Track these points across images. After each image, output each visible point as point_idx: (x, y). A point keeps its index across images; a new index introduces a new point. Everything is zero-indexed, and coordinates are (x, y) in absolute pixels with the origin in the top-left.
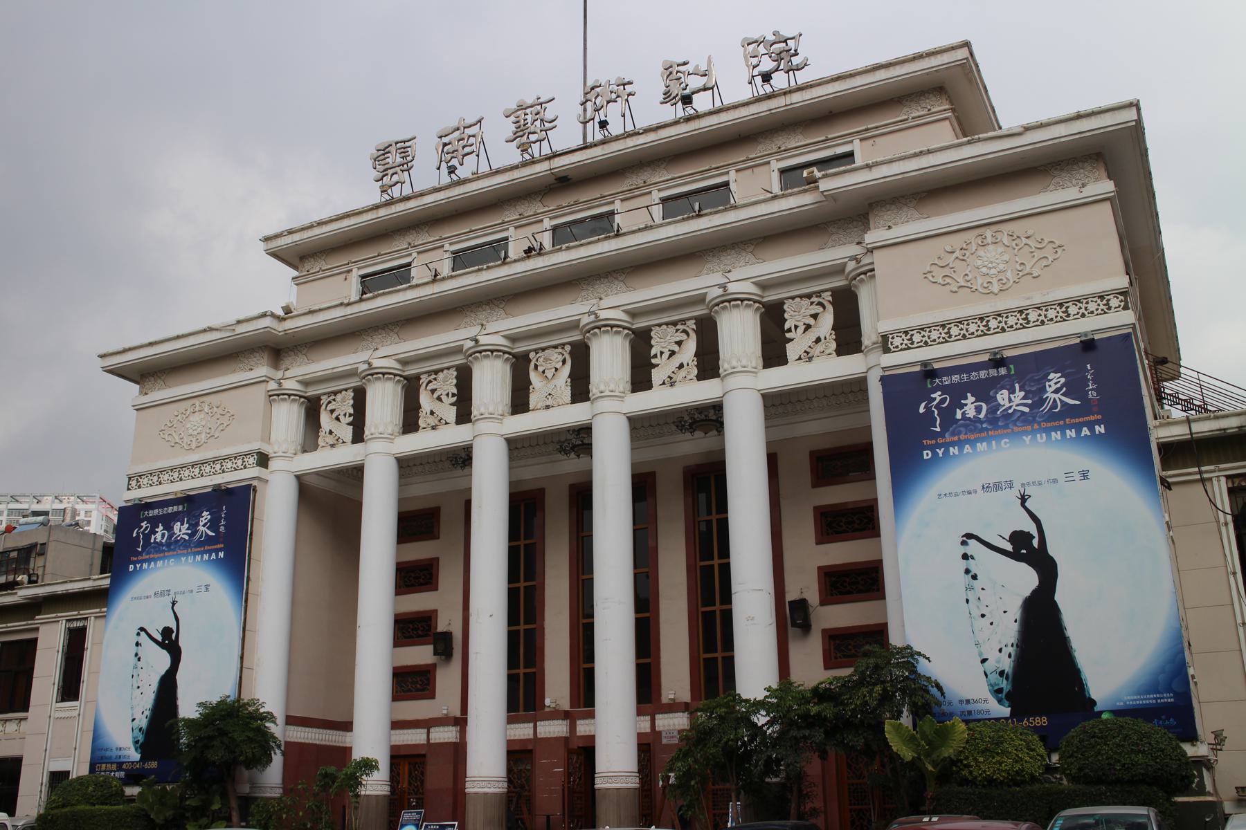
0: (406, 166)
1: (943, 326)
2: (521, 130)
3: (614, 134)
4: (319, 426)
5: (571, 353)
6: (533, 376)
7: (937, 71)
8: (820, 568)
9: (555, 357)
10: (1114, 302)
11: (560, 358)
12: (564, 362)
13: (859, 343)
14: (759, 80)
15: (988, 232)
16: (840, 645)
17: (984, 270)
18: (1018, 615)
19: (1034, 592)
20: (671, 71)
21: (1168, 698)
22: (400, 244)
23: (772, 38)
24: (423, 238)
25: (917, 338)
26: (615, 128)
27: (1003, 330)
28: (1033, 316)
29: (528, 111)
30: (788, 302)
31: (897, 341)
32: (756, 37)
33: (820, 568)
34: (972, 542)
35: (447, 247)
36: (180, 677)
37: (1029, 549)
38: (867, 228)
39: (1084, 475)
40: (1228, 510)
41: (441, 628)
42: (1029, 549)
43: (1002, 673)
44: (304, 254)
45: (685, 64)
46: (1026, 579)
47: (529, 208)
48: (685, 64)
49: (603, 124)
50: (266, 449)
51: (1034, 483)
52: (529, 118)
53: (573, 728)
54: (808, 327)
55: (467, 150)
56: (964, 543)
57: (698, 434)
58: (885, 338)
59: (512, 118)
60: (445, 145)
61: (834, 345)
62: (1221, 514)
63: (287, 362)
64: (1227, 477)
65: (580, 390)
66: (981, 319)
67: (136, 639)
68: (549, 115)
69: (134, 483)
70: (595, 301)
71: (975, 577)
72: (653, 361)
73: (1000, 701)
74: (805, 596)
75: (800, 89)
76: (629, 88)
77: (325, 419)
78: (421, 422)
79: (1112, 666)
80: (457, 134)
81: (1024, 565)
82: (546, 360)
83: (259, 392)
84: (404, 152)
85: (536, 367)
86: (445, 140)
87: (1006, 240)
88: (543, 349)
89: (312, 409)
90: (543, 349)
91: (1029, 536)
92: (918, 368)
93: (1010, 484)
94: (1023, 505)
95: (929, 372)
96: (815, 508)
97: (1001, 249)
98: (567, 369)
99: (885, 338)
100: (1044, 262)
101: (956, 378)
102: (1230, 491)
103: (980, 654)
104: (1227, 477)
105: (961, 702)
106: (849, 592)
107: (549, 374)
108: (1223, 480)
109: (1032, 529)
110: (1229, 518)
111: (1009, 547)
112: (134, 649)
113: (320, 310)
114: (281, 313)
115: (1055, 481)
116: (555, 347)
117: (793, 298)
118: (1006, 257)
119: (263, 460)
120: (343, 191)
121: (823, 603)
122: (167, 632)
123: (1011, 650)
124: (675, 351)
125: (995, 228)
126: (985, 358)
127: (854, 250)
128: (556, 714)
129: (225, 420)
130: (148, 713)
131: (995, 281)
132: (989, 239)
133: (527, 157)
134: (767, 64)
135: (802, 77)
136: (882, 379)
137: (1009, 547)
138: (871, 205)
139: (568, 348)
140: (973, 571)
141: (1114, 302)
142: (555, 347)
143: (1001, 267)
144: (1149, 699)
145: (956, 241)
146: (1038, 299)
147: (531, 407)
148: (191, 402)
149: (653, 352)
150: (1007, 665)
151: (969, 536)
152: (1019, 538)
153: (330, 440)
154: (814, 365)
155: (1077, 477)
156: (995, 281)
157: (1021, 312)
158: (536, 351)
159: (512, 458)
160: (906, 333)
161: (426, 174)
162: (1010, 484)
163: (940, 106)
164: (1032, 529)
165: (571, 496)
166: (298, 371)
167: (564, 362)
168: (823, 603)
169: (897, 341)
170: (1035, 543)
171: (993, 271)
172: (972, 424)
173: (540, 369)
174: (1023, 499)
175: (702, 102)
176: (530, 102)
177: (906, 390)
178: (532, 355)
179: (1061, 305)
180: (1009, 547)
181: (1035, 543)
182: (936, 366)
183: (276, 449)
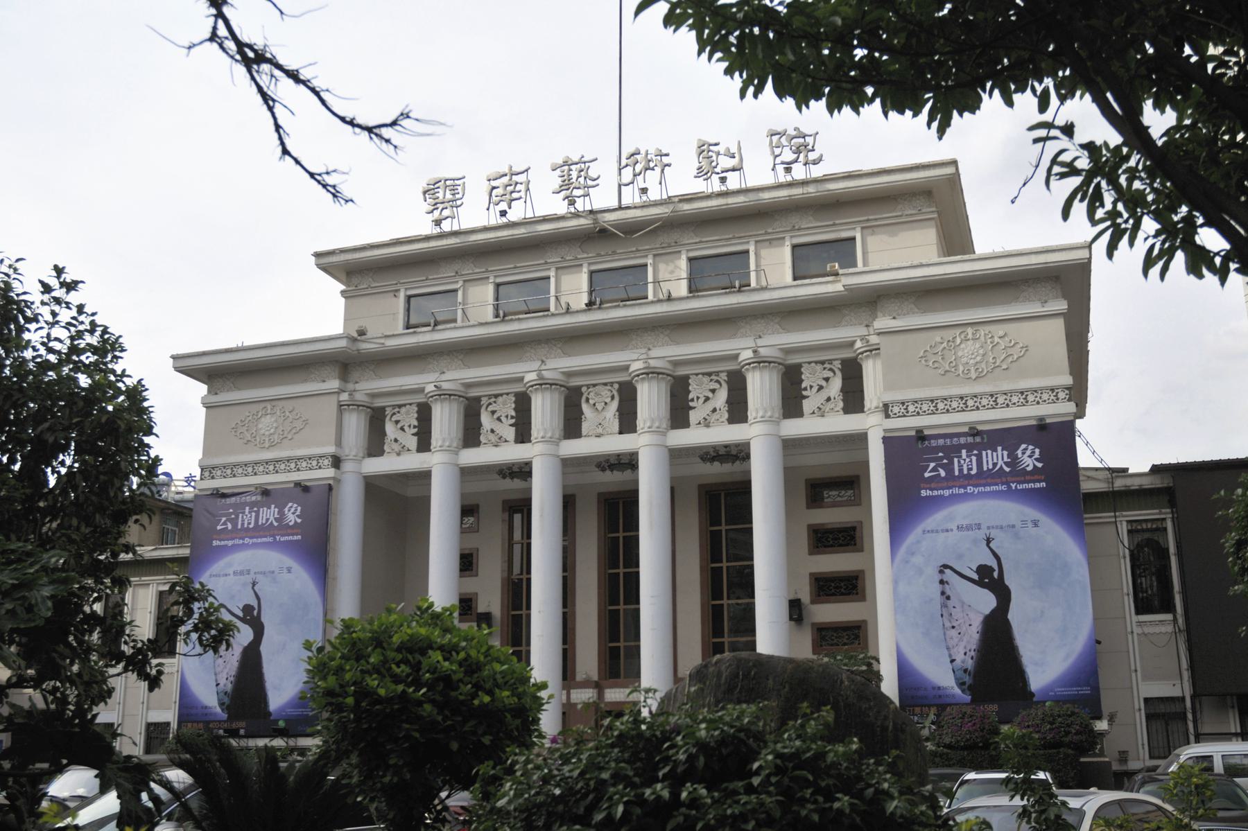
0: (454, 204)
1: (932, 401)
2: (566, 185)
3: (652, 199)
4: (384, 434)
5: (619, 391)
6: (584, 407)
7: (929, 181)
8: (811, 574)
9: (605, 393)
10: (1062, 395)
11: (609, 394)
12: (613, 398)
13: (863, 406)
14: (780, 168)
15: (970, 330)
16: (826, 636)
18: (979, 629)
19: (993, 612)
20: (705, 149)
21: (1086, 691)
22: (447, 271)
23: (792, 132)
24: (469, 269)
25: (911, 408)
26: (654, 195)
27: (978, 408)
28: (1001, 400)
29: (573, 167)
30: (805, 366)
31: (896, 410)
32: (780, 129)
33: (811, 574)
34: (948, 571)
36: (264, 648)
37: (990, 578)
38: (875, 318)
39: (289, 570)
40: (1126, 544)
41: (481, 608)
42: (990, 578)
43: (965, 671)
44: (356, 270)
45: (716, 144)
46: (986, 601)
47: (570, 253)
48: (716, 144)
49: (644, 191)
50: (340, 453)
52: (574, 174)
53: (601, 695)
54: (821, 388)
55: (515, 195)
56: (941, 572)
57: (716, 463)
58: (886, 406)
59: (558, 172)
60: (494, 188)
61: (841, 404)
62: (1121, 546)
63: (355, 375)
64: (1128, 522)
65: (628, 423)
66: (962, 398)
68: (592, 174)
69: (207, 474)
70: (643, 351)
72: (691, 404)
74: (799, 596)
75: (816, 181)
76: (665, 160)
77: (390, 429)
78: (482, 439)
79: (1046, 663)
80: (505, 180)
81: (986, 591)
82: (597, 394)
83: (332, 403)
84: (454, 189)
85: (587, 400)
86: (494, 183)
88: (594, 385)
89: (376, 420)
90: (594, 385)
91: (991, 569)
92: (913, 433)
93: (979, 526)
94: (988, 545)
95: (921, 436)
96: (809, 526)
98: (615, 405)
99: (886, 406)
101: (941, 442)
102: (1129, 532)
103: (950, 656)
104: (1128, 522)
105: (934, 688)
106: (833, 595)
107: (599, 407)
108: (1125, 524)
109: (995, 565)
110: (1127, 551)
111: (976, 577)
113: (394, 335)
114: (355, 335)
115: (1013, 526)
116: (605, 384)
117: (810, 363)
119: (337, 462)
120: (390, 213)
121: (813, 602)
123: (973, 653)
124: (709, 400)
126: (966, 429)
127: (862, 331)
128: (585, 684)
129: (299, 424)
131: (973, 369)
133: (572, 210)
134: (788, 156)
135: (817, 172)
136: (885, 440)
138: (879, 297)
139: (616, 386)
141: (1062, 395)
142: (605, 384)
144: (1073, 691)
145: (949, 334)
146: (1006, 387)
147: (584, 432)
148: (262, 405)
149: (690, 397)
152: (983, 570)
154: (823, 420)
155: (1030, 525)
156: (973, 369)
157: (992, 396)
158: (588, 386)
159: (564, 474)
160: (903, 404)
161: (475, 214)
162: (979, 526)
163: (930, 212)
164: (995, 565)
165: (599, 502)
166: (369, 385)
167: (613, 398)
168: (813, 602)
169: (896, 410)
170: (996, 575)
172: (967, 479)
173: (591, 402)
174: (988, 541)
175: (734, 182)
176: (576, 159)
177: (908, 452)
178: (584, 389)
179: (1022, 393)
180: (976, 577)
181: (996, 575)
182: (926, 432)
183: (347, 452)
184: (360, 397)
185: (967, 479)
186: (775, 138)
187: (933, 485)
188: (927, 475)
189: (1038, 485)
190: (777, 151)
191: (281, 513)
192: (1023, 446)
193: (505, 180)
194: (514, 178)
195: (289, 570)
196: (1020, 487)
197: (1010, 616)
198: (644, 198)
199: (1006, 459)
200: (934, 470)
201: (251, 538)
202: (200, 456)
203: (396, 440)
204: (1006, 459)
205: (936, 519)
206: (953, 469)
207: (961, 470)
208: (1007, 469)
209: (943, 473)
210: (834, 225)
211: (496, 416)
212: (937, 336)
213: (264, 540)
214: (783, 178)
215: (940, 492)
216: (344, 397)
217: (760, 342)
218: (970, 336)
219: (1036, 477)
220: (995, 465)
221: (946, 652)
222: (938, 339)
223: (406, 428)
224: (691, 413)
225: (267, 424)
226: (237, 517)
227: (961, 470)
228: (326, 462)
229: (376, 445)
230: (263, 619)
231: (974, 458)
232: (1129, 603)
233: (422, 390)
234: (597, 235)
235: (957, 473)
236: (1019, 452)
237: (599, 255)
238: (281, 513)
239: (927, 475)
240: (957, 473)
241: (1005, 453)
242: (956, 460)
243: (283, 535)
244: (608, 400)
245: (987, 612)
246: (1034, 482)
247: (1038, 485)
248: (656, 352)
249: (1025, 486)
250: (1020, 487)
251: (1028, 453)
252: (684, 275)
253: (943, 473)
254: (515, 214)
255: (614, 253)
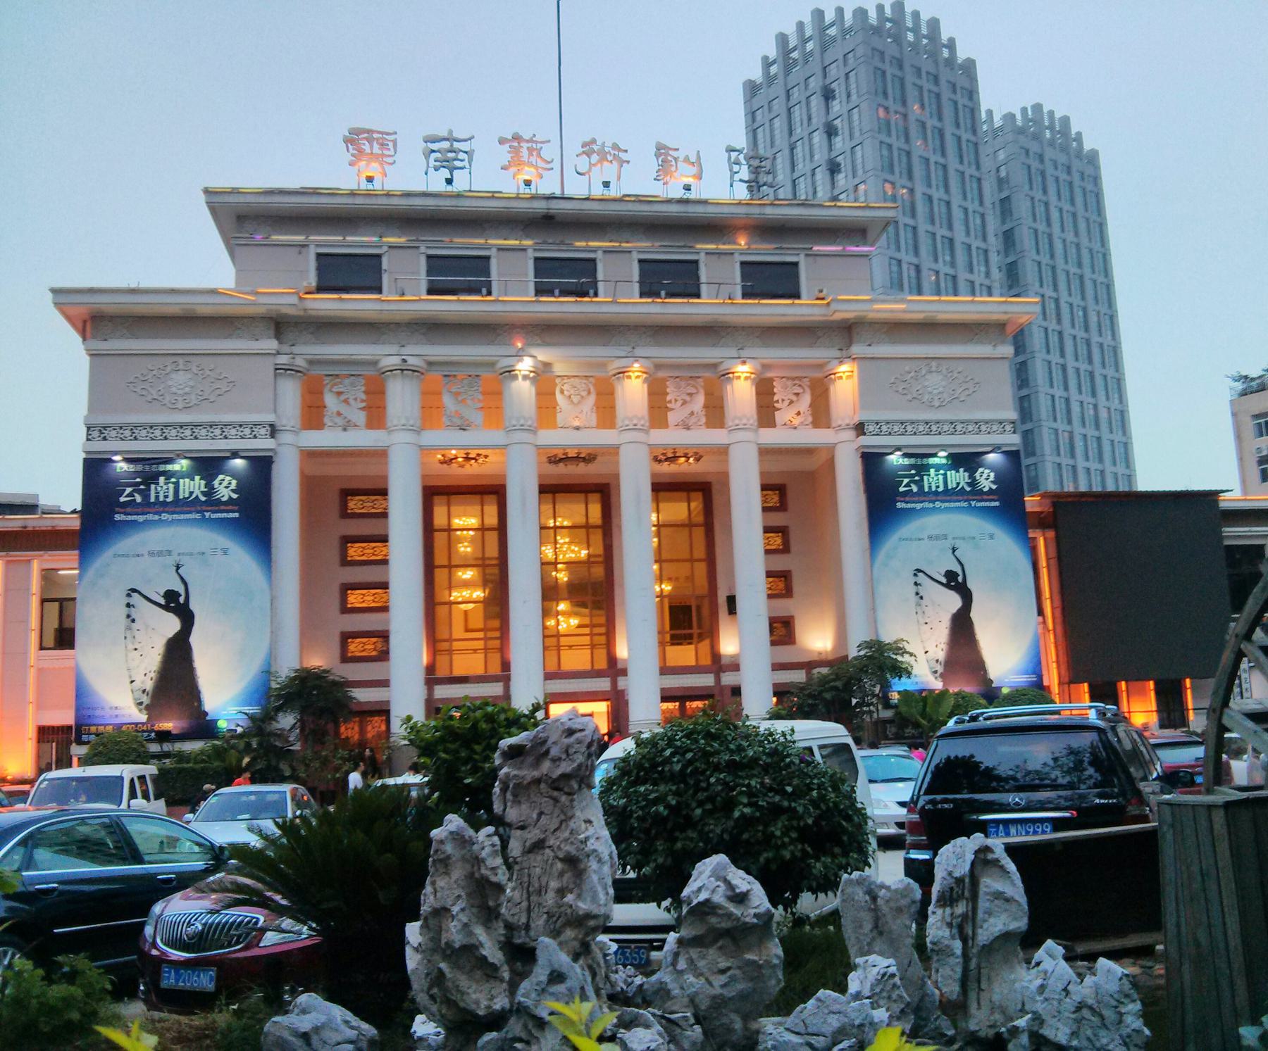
6: (558, 396)
12: (589, 393)
17: (174, 390)
19: (177, 635)
35: (423, 249)
39: (225, 551)
42: (177, 604)
43: (144, 691)
51: (187, 554)
56: (129, 595)
61: (704, 420)
67: (126, 600)
69: (95, 434)
71: (133, 621)
73: (140, 710)
78: (326, 420)
80: (446, 145)
83: (268, 365)
86: (435, 146)
87: (195, 370)
93: (169, 553)
97: (189, 376)
100: (218, 392)
107: (575, 399)
109: (181, 590)
111: (162, 601)
112: (125, 610)
118: (191, 383)
122: (951, 575)
125: (188, 358)
130: (153, 675)
132: (181, 367)
137: (162, 601)
140: (133, 617)
143: (187, 390)
148: (175, 358)
150: (149, 685)
151: (134, 590)
152: (171, 596)
153: (339, 421)
155: (219, 552)
162: (169, 553)
164: (181, 590)
166: (309, 350)
171: (180, 392)
172: (163, 506)
180: (944, 581)
183: (284, 422)
184: (300, 362)
185: (163, 506)
186: (734, 155)
187: (128, 510)
188: (122, 499)
189: (231, 515)
190: (736, 168)
191: (209, 485)
192: (221, 477)
193: (446, 145)
194: (456, 145)
195: (992, 536)
196: (979, 504)
197: (972, 615)
198: (449, 188)
199: (203, 489)
200: (130, 495)
201: (943, 501)
202: (85, 412)
203: (339, 414)
204: (203, 489)
205: (908, 529)
206: (149, 496)
207: (157, 497)
208: (203, 499)
209: (138, 499)
210: (781, 248)
211: (343, 397)
212: (907, 366)
213: (957, 504)
214: (364, 186)
215: (913, 505)
216: (283, 360)
217: (405, 351)
218: (934, 369)
219: (230, 508)
220: (191, 493)
221: (126, 673)
222: (907, 368)
223: (351, 401)
224: (670, 414)
225: (180, 380)
226: (922, 480)
227: (157, 497)
228: (871, 428)
229: (313, 416)
230: (970, 585)
231: (171, 486)
232: (34, 638)
233: (375, 363)
234: (546, 221)
235: (152, 500)
236: (216, 483)
237: (545, 242)
238: (209, 485)
239: (902, 489)
240: (152, 500)
241: (203, 482)
242: (153, 487)
243: (214, 512)
244: (584, 394)
245: (171, 635)
246: (228, 511)
247: (231, 515)
248: (409, 349)
249: (983, 504)
250: (979, 504)
251: (225, 484)
252: (636, 277)
253: (138, 499)
254: (461, 184)
255: (562, 243)
